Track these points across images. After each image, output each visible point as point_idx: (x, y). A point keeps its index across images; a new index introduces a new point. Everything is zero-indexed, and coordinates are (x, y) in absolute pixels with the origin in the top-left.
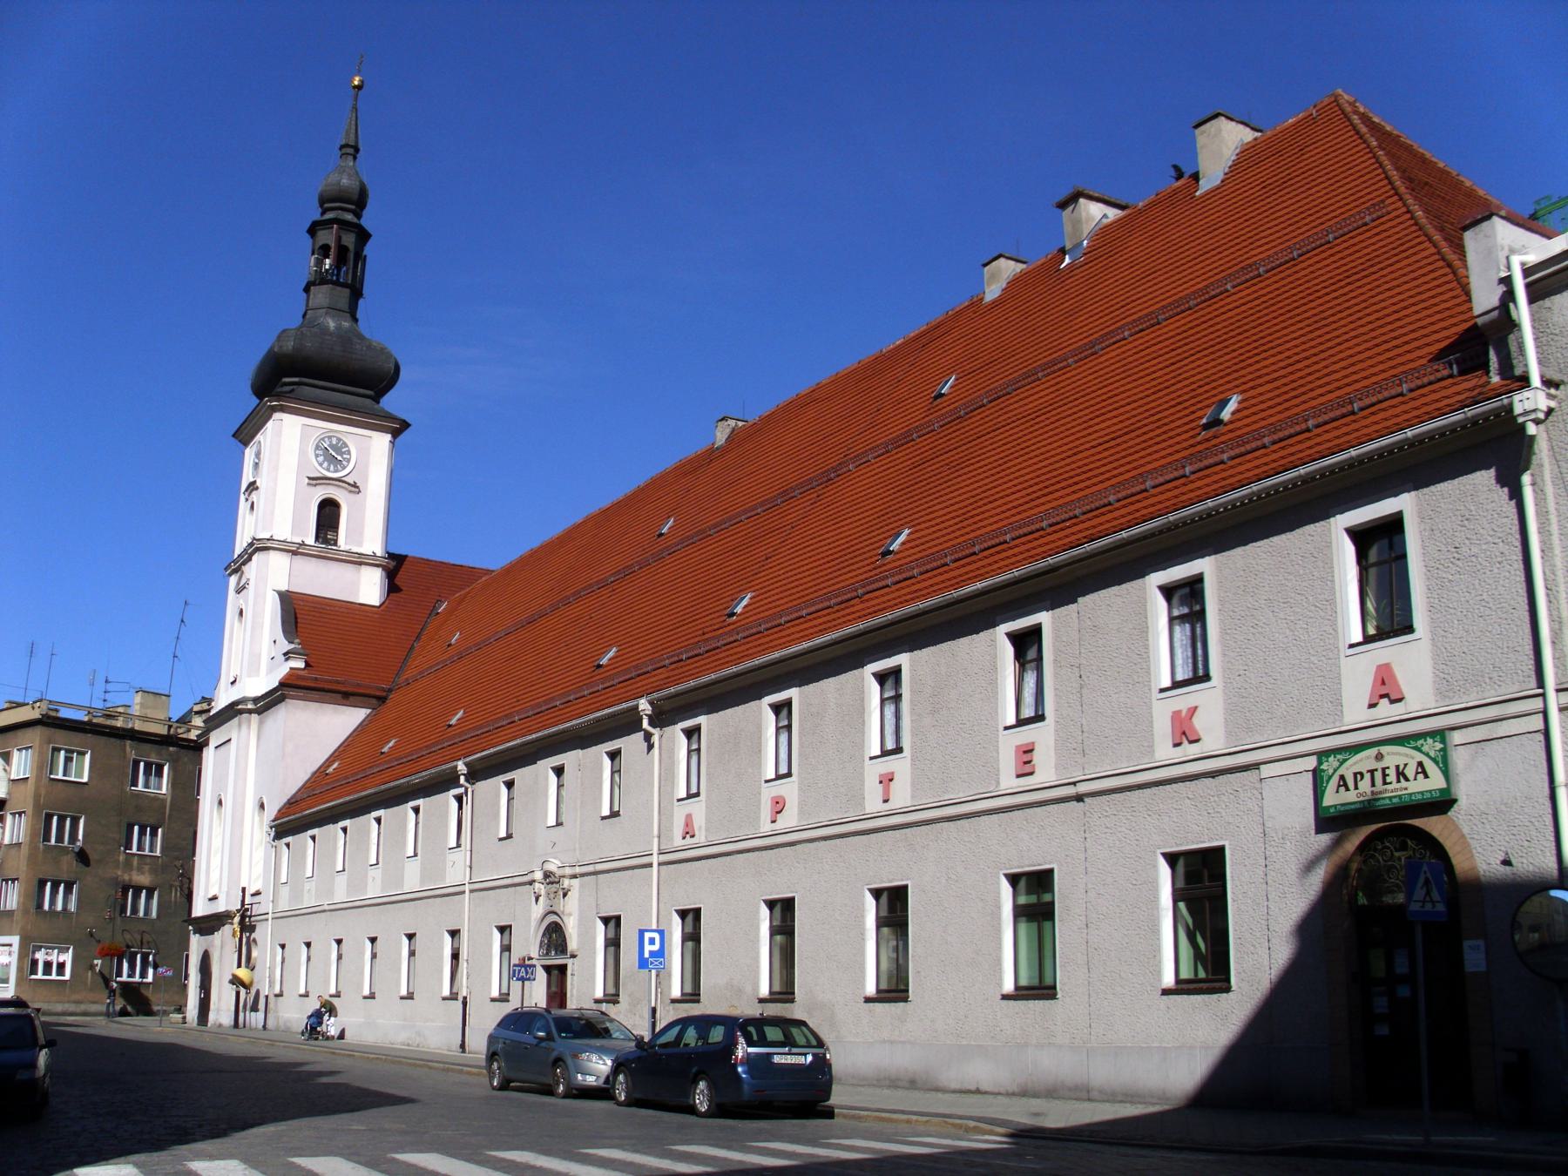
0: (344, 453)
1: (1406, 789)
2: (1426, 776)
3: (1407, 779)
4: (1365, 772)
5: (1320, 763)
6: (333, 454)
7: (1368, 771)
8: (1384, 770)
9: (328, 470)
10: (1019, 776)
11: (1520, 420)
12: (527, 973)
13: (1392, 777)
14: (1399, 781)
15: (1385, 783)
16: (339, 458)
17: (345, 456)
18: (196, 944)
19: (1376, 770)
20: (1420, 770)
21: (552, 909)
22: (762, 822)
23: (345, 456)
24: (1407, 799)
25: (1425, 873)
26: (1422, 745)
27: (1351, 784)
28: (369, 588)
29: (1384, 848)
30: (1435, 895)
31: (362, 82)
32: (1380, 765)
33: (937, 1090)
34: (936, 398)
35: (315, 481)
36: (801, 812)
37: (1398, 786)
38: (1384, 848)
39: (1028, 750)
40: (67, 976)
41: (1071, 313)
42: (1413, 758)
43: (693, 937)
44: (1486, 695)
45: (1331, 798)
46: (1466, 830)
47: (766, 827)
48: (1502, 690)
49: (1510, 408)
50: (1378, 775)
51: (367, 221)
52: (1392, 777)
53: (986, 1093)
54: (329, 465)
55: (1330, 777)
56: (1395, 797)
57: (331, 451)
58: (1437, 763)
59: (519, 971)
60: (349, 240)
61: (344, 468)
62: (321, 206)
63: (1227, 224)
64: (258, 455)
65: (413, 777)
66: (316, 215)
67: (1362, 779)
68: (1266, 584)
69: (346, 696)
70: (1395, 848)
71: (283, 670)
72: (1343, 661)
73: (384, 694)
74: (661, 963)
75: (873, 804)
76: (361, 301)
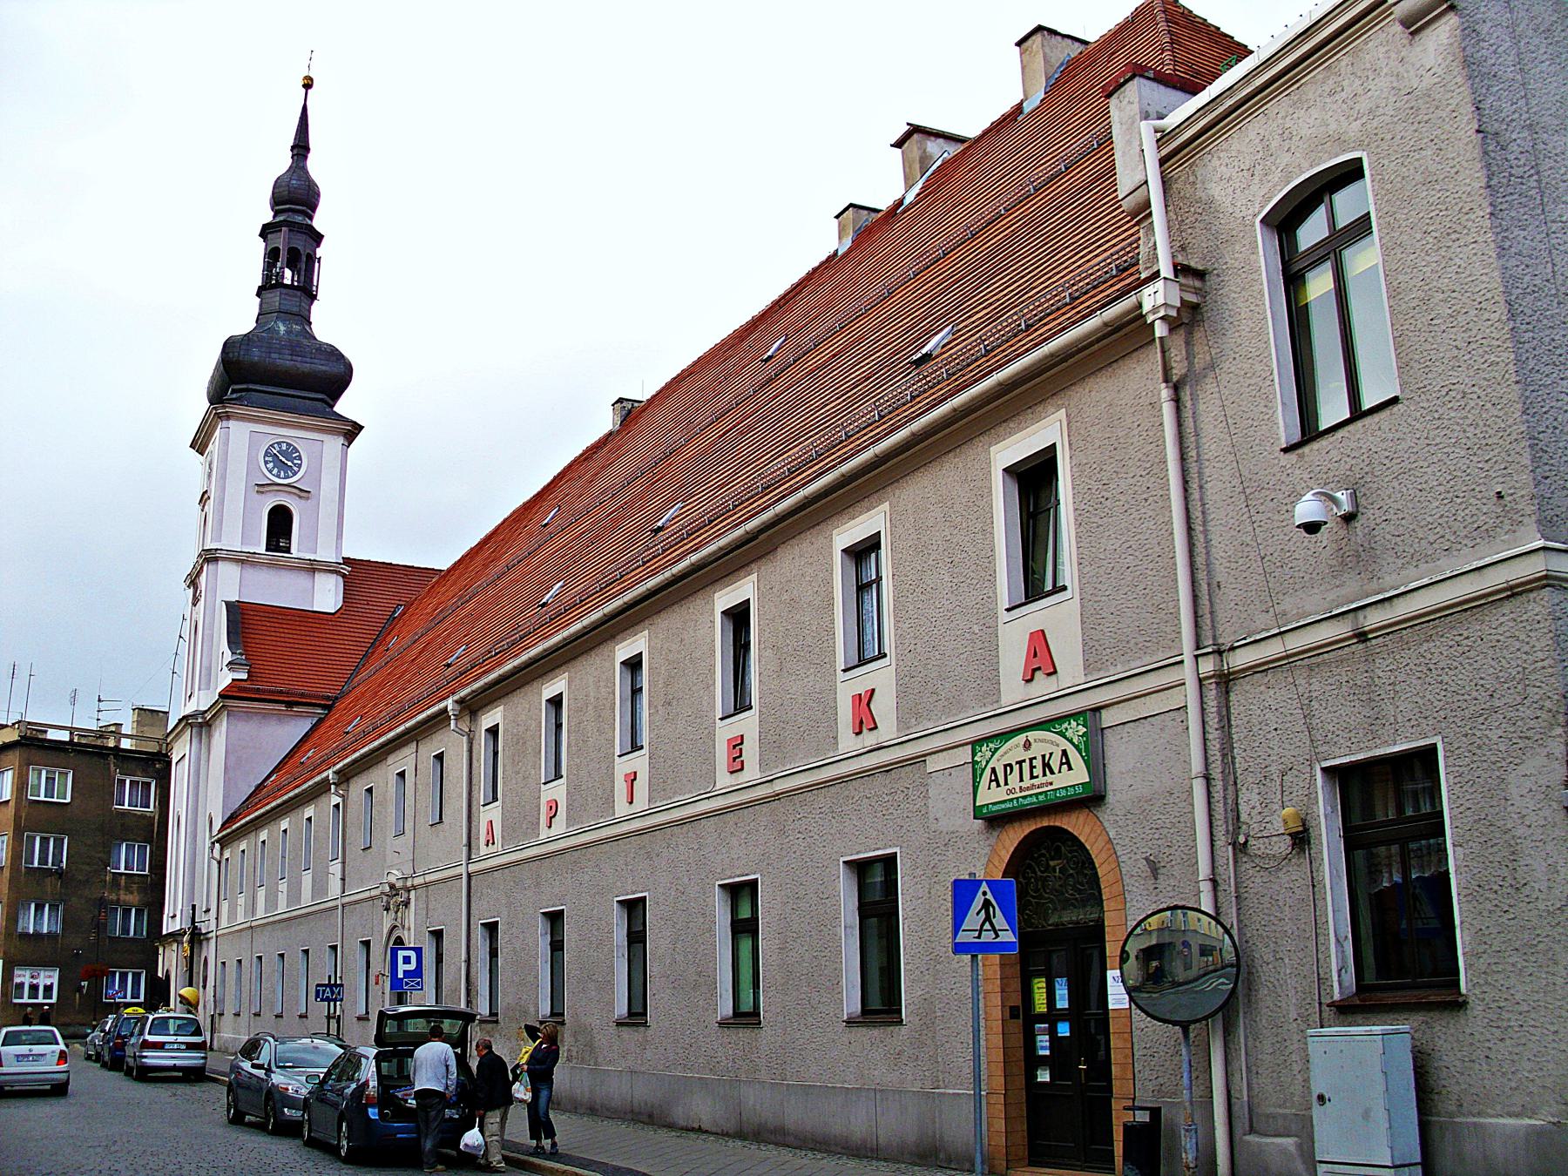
0: (295, 458)
1: (1051, 784)
2: (1070, 768)
3: (1052, 772)
4: (1014, 764)
5: (974, 755)
6: (283, 460)
7: (1017, 763)
8: (1031, 760)
9: (278, 476)
10: (732, 773)
12: (333, 993)
13: (1038, 771)
14: (1044, 775)
15: (1032, 777)
16: (290, 464)
17: (295, 462)
19: (1024, 761)
20: (1064, 761)
23: (295, 462)
24: (1051, 796)
25: (985, 893)
26: (1066, 729)
27: (1002, 782)
30: (999, 920)
32: (1030, 754)
35: (262, 488)
36: (570, 820)
40: (54, 1000)
42: (1058, 745)
45: (990, 795)
47: (544, 834)
48: (1147, 659)
50: (1026, 766)
52: (1038, 771)
53: (706, 1132)
54: (279, 472)
55: (983, 770)
56: (1041, 793)
57: (281, 458)
59: (324, 991)
60: (300, 243)
61: (295, 474)
66: (268, 216)
69: (292, 703)
71: (225, 679)
74: (418, 983)
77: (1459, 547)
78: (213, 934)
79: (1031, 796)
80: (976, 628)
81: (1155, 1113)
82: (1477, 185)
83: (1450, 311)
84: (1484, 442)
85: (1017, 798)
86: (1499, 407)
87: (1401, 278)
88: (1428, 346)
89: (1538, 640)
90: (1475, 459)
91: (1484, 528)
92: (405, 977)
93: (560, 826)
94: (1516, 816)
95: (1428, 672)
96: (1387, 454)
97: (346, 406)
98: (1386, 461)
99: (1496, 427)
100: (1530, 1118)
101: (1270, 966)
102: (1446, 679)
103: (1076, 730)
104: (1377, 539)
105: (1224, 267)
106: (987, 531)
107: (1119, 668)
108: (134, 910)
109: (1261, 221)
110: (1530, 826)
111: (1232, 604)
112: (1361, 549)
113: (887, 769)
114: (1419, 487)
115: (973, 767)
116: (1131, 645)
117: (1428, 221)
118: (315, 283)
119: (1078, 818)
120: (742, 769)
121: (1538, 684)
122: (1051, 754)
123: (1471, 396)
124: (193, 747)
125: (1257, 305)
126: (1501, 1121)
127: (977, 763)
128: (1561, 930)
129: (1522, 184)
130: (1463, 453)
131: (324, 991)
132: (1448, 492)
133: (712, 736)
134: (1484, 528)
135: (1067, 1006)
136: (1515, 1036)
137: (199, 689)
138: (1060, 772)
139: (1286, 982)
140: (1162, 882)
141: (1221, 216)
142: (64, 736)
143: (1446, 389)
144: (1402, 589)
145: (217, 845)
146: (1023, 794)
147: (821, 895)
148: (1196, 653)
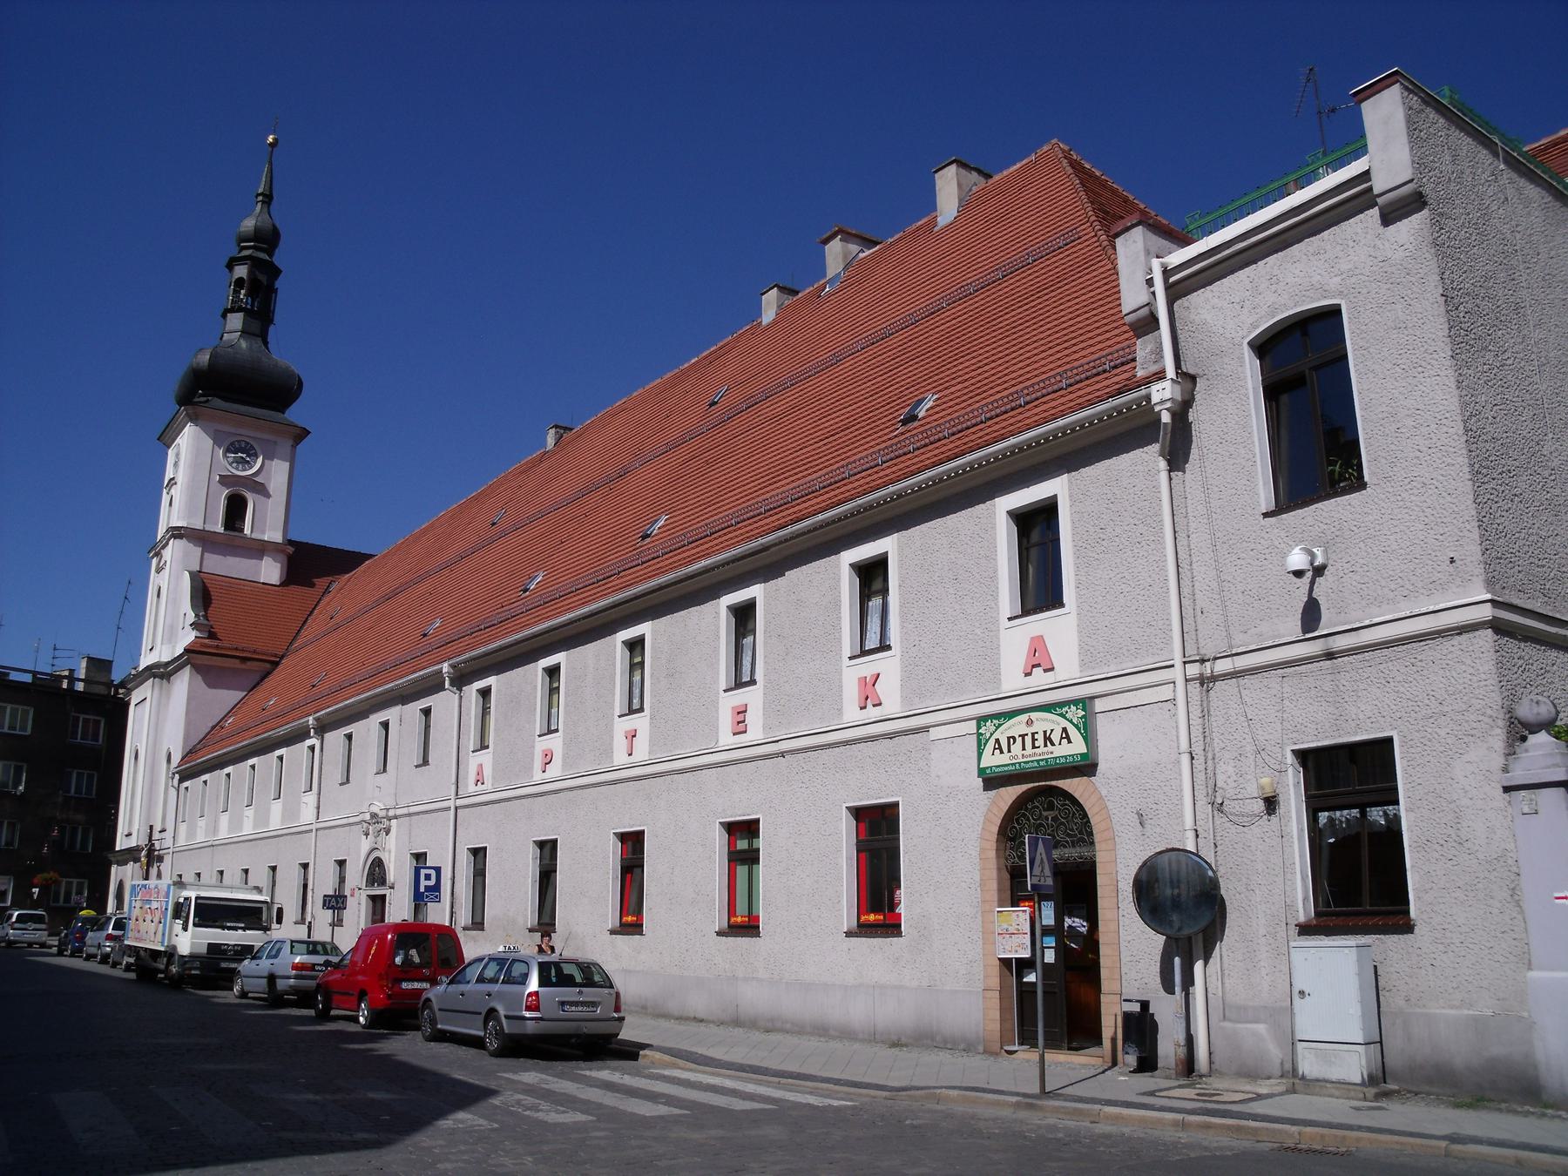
1: (1052, 753)
2: (1069, 742)
3: (1053, 744)
4: (1017, 737)
5: (979, 728)
7: (1020, 736)
8: (1033, 734)
9: (237, 469)
11: (1157, 409)
12: (337, 903)
13: (1041, 742)
14: (1046, 746)
15: (1034, 747)
18: (116, 872)
19: (1027, 735)
21: (376, 846)
22: (535, 772)
26: (1067, 712)
27: (1005, 748)
28: (270, 571)
29: (1034, 807)
31: (276, 140)
32: (1029, 730)
33: (666, 1016)
34: (711, 405)
36: (565, 764)
37: (1045, 749)
38: (1034, 807)
39: (742, 711)
41: (980, 384)
43: (479, 874)
44: (1124, 666)
45: (991, 760)
46: (1104, 793)
47: (538, 776)
48: (1138, 662)
49: (1148, 398)
50: (1028, 740)
51: (278, 259)
55: (987, 741)
56: (1042, 760)
58: (1079, 729)
59: (330, 901)
62: (239, 245)
63: (953, 253)
64: (177, 455)
65: (278, 730)
67: (1014, 743)
68: (939, 562)
70: (1043, 807)
72: (1002, 631)
73: (278, 659)
74: (436, 897)
75: (620, 758)
76: (272, 328)
77: (1417, 594)
78: (170, 850)
79: (1032, 761)
80: (978, 631)
81: (1145, 1005)
82: (1441, 334)
83: (1414, 424)
84: (1439, 520)
85: (1020, 763)
86: (1454, 496)
87: (1372, 396)
88: (1393, 447)
89: (1482, 665)
90: (1432, 532)
91: (1438, 582)
92: (426, 891)
93: (554, 770)
94: (1459, 791)
95: (1386, 684)
96: (1356, 523)
97: (296, 413)
98: (1354, 528)
99: (1451, 511)
100: (1469, 1009)
101: (1242, 895)
102: (1402, 689)
103: (1075, 713)
104: (1345, 584)
105: (1214, 374)
106: (991, 557)
107: (1112, 667)
108: (80, 828)
109: (1248, 343)
110: (1471, 799)
111: (1214, 625)
112: (1331, 591)
113: (891, 736)
114: (1383, 549)
115: (978, 737)
116: (1124, 650)
117: (1397, 356)
118: (272, 308)
119: (1557, 765)
120: (745, 732)
121: (1481, 697)
122: (1052, 730)
123: (1430, 486)
124: (154, 696)
125: (1243, 405)
126: (1444, 1011)
127: (982, 734)
128: (1497, 875)
129: (1467, 335)
130: (1421, 527)
131: (330, 901)
132: (1408, 554)
133: (715, 704)
134: (1438, 582)
135: (1053, 923)
136: (1456, 950)
137: (162, 644)
138: (1060, 744)
139: (1256, 907)
140: (1149, 829)
141: (1213, 335)
142: (28, 678)
143: (1408, 480)
144: (1367, 622)
145: (177, 775)
146: (1025, 760)
147: (823, 833)
148: (1184, 660)
